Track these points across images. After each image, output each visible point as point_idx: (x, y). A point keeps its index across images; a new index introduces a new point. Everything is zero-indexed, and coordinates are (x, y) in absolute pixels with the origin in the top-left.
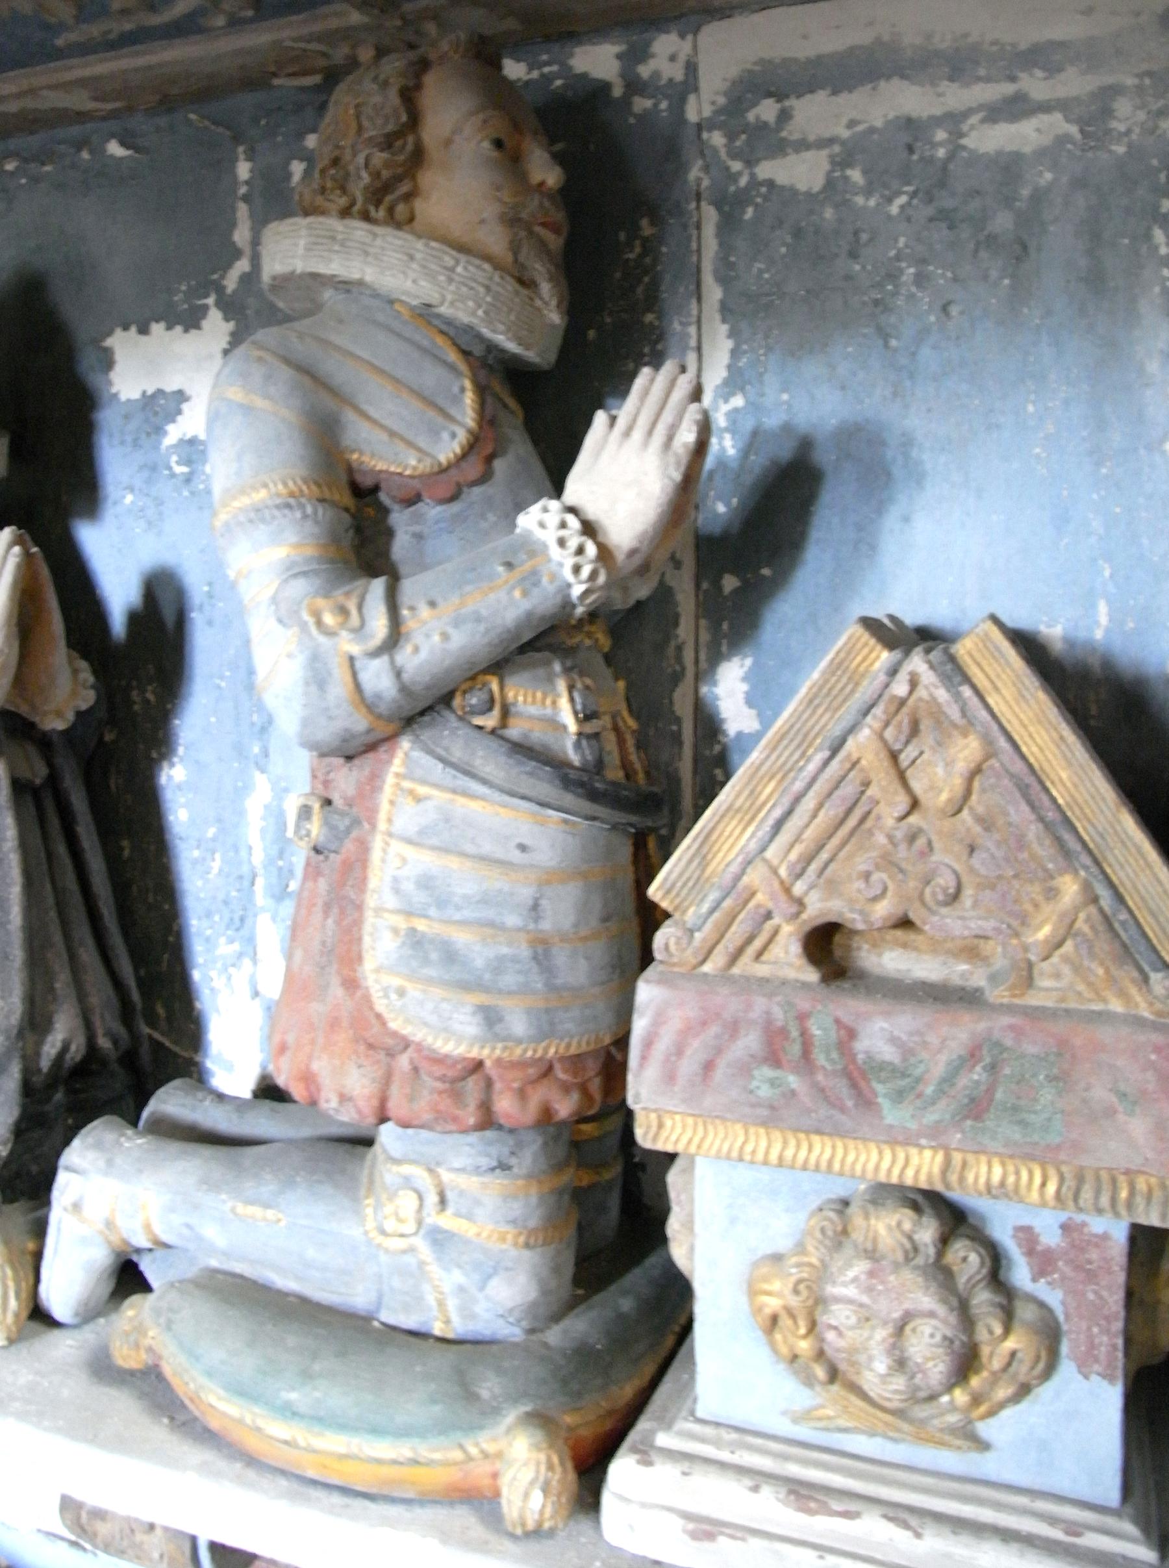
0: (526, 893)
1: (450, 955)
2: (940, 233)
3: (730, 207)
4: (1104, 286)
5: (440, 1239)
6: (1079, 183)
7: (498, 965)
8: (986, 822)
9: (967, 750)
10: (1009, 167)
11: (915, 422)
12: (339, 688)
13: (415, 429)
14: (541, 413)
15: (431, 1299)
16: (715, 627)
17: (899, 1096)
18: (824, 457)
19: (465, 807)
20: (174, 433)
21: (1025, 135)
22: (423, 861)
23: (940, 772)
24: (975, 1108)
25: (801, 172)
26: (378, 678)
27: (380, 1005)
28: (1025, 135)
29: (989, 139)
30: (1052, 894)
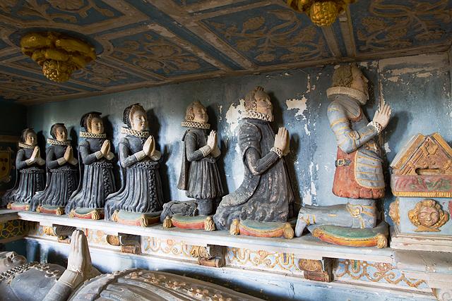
0: (374, 169)
1: (366, 176)
2: (414, 87)
3: (384, 84)
4: (437, 95)
5: (362, 215)
6: (433, 81)
7: (372, 178)
8: (438, 155)
9: (435, 147)
10: (423, 79)
11: (412, 111)
12: (353, 144)
13: (355, 114)
14: (367, 110)
15: (361, 224)
16: (384, 138)
17: (430, 186)
18: (399, 116)
19: (366, 159)
20: (297, 115)
21: (425, 75)
22: (362, 165)
23: (432, 150)
24: (439, 187)
25: (395, 79)
26: (358, 142)
27: (358, 183)
28: (425, 75)
29: (420, 76)
30: (447, 162)
